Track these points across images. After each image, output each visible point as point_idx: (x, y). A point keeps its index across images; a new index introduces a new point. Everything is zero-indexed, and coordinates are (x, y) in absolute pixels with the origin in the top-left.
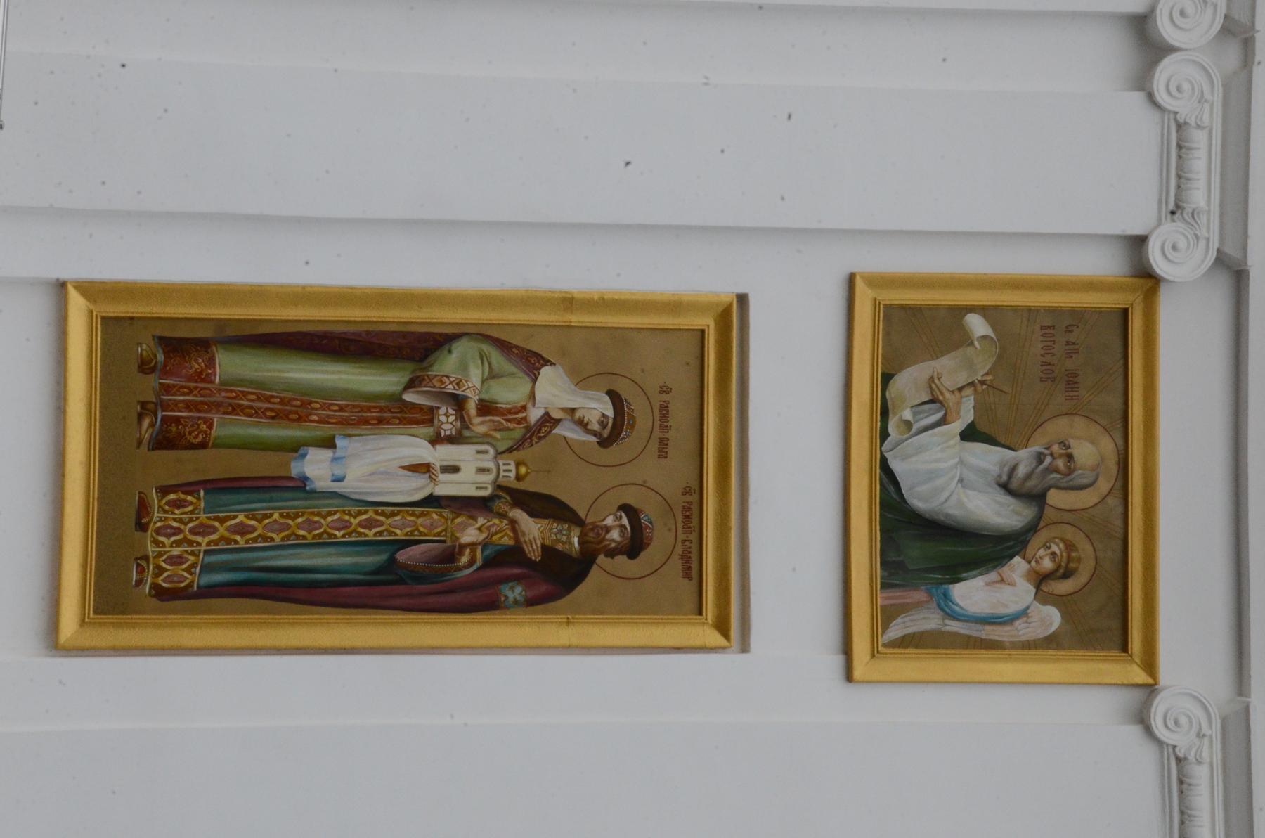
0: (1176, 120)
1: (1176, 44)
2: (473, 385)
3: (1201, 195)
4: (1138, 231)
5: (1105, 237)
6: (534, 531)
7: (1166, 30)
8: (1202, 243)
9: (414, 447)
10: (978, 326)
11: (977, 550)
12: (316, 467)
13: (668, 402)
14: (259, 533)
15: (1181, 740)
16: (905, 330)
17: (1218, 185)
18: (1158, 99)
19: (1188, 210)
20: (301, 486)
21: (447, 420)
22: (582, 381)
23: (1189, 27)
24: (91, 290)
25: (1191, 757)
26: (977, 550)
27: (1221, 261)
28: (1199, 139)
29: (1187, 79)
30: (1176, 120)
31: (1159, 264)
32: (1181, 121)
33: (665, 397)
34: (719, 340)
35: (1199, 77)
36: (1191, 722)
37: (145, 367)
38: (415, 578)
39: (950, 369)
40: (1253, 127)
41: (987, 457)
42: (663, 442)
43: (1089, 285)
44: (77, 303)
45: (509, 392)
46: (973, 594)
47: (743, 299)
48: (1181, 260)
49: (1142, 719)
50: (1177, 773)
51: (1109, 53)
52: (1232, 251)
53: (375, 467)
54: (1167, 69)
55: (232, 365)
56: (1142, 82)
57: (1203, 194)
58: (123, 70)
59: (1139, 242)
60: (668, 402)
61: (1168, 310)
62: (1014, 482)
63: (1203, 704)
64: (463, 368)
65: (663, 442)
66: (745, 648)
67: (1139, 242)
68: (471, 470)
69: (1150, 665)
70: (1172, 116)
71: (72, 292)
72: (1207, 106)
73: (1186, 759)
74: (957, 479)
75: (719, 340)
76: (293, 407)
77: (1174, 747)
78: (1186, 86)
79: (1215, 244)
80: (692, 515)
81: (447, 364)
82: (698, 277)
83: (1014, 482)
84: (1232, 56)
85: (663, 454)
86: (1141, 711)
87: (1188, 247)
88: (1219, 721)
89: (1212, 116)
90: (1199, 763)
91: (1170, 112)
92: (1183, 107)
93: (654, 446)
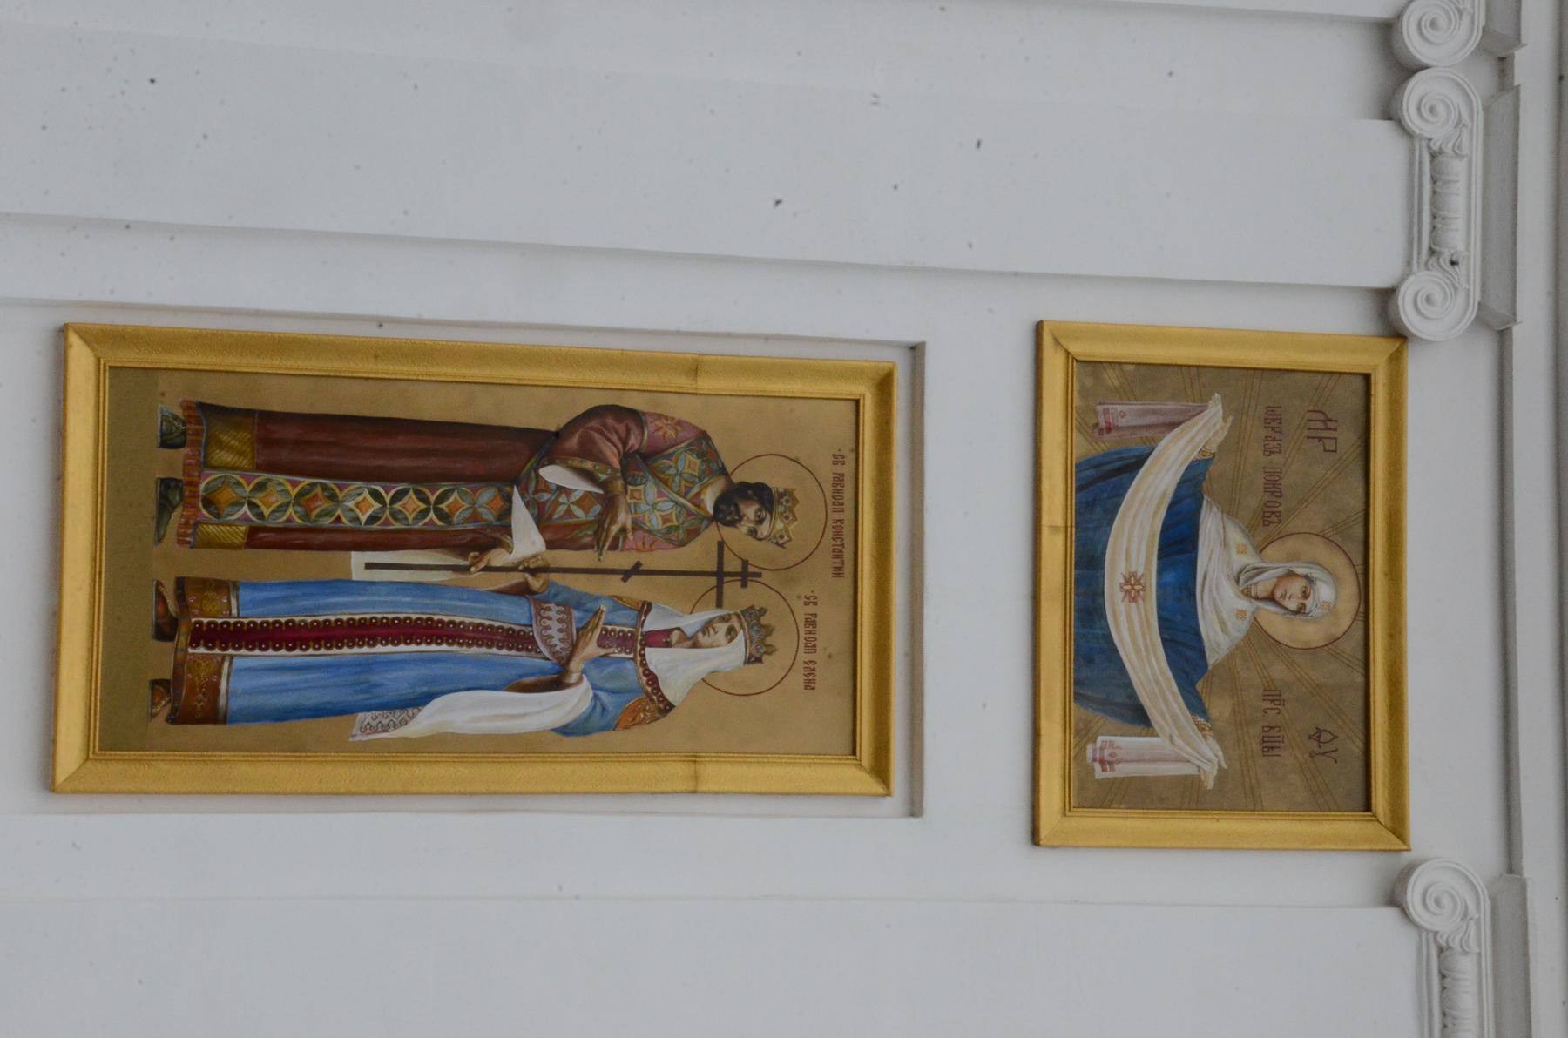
0: (1429, 147)
1: (1424, 60)
3: (1461, 236)
4: (1382, 282)
5: (1332, 20)
7: (1415, 44)
8: (1461, 296)
13: (815, 615)
15: (1441, 922)
17: (1479, 222)
18: (1418, 919)
19: (1446, 256)
23: (1444, 47)
24: (98, 338)
25: (1448, 149)
27: (1482, 320)
28: (1457, 169)
30: (1429, 147)
31: (1409, 317)
32: (1443, 943)
33: (811, 609)
34: (889, 393)
35: (1457, 98)
36: (1455, 903)
40: (1519, 268)
42: (810, 671)
44: (81, 360)
47: (916, 351)
48: (1437, 312)
49: (1393, 898)
50: (1440, 964)
51: (1348, 68)
52: (1498, 306)
54: (1416, 88)
57: (1461, 236)
58: (153, 76)
59: (1385, 297)
60: (815, 615)
61: (1419, 371)
62: (1227, 582)
63: (1463, 89)
65: (810, 671)
66: (914, 808)
67: (1385, 297)
69: (1398, 826)
70: (1424, 143)
71: (74, 339)
72: (1472, 925)
73: (1449, 948)
75: (889, 393)
77: (1436, 933)
78: (1446, 900)
79: (1481, 21)
80: (842, 494)
82: (867, 320)
83: (1227, 582)
85: (809, 685)
86: (1393, 891)
87: (1445, 298)
88: (1488, 903)
89: (1474, 146)
90: (1465, 953)
91: (1428, 931)
93: (797, 679)
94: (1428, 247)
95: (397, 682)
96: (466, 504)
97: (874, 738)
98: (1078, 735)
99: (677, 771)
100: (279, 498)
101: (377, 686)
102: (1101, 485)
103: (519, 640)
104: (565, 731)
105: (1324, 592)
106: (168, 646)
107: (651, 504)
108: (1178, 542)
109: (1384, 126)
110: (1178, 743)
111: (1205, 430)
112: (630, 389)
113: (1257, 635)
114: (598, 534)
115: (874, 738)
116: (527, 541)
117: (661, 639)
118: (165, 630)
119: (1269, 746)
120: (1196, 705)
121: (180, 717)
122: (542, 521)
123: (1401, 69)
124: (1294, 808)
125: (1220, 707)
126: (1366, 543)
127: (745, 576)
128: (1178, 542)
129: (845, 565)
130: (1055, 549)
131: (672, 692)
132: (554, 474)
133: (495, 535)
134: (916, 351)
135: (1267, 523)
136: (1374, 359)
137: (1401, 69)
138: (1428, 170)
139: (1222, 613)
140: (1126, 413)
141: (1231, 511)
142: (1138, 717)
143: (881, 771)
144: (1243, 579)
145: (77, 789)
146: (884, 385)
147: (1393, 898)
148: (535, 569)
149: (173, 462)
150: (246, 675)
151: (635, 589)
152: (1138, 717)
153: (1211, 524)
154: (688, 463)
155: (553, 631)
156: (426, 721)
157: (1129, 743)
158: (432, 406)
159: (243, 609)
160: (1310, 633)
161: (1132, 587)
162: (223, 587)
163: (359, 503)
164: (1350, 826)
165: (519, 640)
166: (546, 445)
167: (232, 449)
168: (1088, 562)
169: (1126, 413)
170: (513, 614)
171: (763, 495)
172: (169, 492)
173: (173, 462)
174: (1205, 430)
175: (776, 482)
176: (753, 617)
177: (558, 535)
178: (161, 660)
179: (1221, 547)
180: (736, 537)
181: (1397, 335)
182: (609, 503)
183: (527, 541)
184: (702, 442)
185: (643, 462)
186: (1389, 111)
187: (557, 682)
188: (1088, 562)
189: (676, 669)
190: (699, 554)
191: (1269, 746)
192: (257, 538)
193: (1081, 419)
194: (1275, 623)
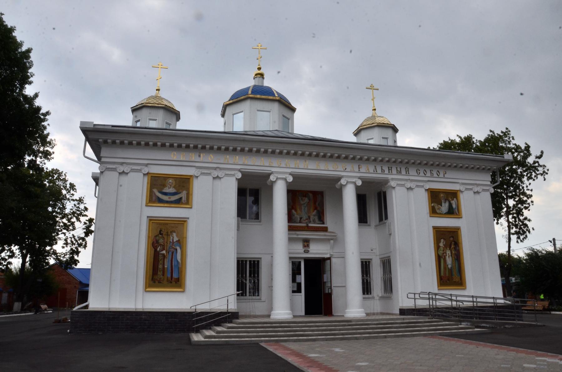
2: (442, 252)
3: (139, 168)
6: (453, 246)
9: (447, 257)
10: (433, 205)
11: (450, 205)
12: (450, 266)
14: (455, 272)
16: (434, 212)
20: (451, 268)
21: (445, 254)
22: (440, 242)
24: (146, 288)
26: (450, 205)
29: (126, 169)
31: (146, 172)
34: (151, 220)
37: (155, 282)
38: (458, 258)
39: (436, 207)
41: (443, 204)
43: (148, 180)
44: (148, 289)
45: (442, 249)
46: (454, 206)
47: (148, 217)
48: (146, 170)
49: (197, 177)
50: (203, 174)
53: (449, 261)
54: (220, 176)
55: (442, 274)
56: (220, 178)
57: (139, 168)
59: (144, 174)
61: (151, 171)
64: (441, 252)
66: (188, 218)
67: (144, 174)
68: (448, 252)
69: (191, 176)
74: (445, 207)
75: (151, 220)
76: (445, 268)
80: (160, 224)
81: (440, 254)
82: (145, 222)
84: (124, 165)
92: (223, 175)
94: (140, 171)
95: (176, 263)
96: (161, 257)
97: (182, 223)
98: (183, 204)
99: (184, 239)
100: (160, 273)
102: (160, 201)
103: (173, 253)
104: (181, 249)
105: (170, 181)
106: (398, 312)
107: (161, 241)
108: (166, 194)
109: (129, 174)
110: (183, 195)
111: (155, 191)
112: (151, 242)
113: (174, 187)
114: (164, 246)
115: (182, 223)
116: (164, 252)
117: (173, 240)
118: (171, 282)
119: (184, 187)
120: (180, 193)
121: (178, 281)
122: (162, 251)
123: (123, 172)
124: (189, 185)
125: (180, 191)
126: (166, 177)
127: (167, 233)
128: (166, 194)
129: (167, 224)
130: (166, 205)
131: (177, 239)
132: (158, 250)
133: (163, 254)
134: (148, 217)
135: (164, 186)
136: (150, 175)
137: (123, 172)
138: (133, 170)
139: (172, 190)
140: (154, 198)
141: (163, 189)
142: (181, 198)
143: (185, 221)
144: (169, 188)
145: (192, 205)
146: (150, 220)
147: (197, 177)
148: (166, 251)
149: (157, 282)
150: (175, 276)
151: (168, 243)
152: (181, 198)
153: (164, 191)
154: (157, 238)
155: (172, 250)
156: (179, 261)
157: (183, 199)
158: (152, 260)
159: (169, 276)
160: (174, 182)
161: (170, 198)
162: (168, 278)
163: (160, 266)
164: (191, 180)
165: (173, 253)
166: (156, 250)
167: (155, 277)
168: (167, 202)
169: (154, 198)
170: (170, 253)
171: (160, 231)
172: (159, 282)
173: (157, 282)
174: (155, 191)
175: (159, 230)
176: (171, 232)
177: (164, 249)
178: (174, 283)
179: (166, 190)
180: (164, 233)
181: (148, 173)
182: (161, 245)
183: (164, 252)
184: (156, 236)
185: (157, 242)
186: (127, 173)
187: (176, 250)
188: (167, 202)
189: (176, 239)
190: (165, 237)
191: (184, 187)
192: (163, 275)
193: (154, 202)
194: (173, 185)
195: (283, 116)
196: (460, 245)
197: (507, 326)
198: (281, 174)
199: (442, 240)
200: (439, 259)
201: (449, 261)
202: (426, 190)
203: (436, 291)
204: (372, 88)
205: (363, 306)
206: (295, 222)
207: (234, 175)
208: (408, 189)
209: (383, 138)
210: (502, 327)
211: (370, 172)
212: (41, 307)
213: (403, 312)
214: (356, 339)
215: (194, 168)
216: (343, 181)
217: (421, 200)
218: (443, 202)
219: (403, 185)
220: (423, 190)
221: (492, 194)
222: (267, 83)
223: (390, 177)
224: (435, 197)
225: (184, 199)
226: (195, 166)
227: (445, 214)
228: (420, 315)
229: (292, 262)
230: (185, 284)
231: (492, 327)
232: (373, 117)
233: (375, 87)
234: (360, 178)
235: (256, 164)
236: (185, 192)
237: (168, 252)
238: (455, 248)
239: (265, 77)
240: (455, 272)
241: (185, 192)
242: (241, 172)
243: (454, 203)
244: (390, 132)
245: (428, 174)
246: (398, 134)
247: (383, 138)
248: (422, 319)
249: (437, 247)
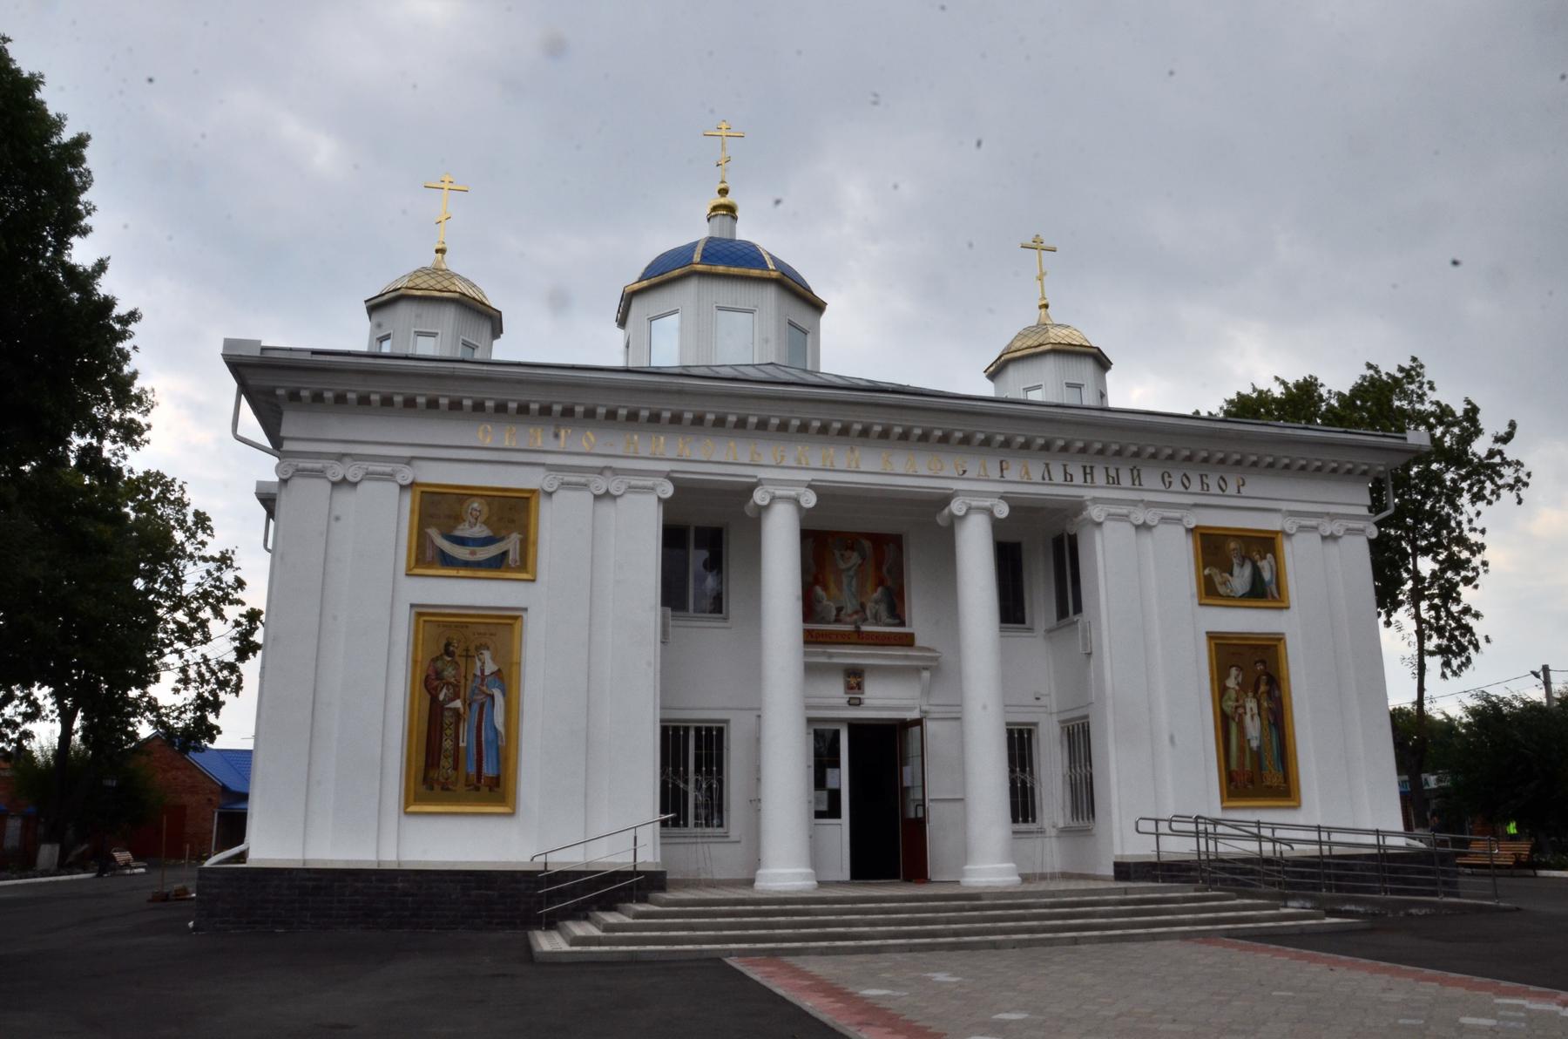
2: (1232, 704)
3: (387, 468)
6: (1263, 688)
9: (1248, 718)
10: (1207, 572)
11: (1257, 573)
12: (1254, 744)
14: (1270, 760)
16: (1210, 592)
20: (1259, 747)
21: (1241, 711)
22: (1228, 676)
24: (407, 804)
26: (1257, 573)
29: (352, 471)
31: (408, 482)
34: (422, 614)
37: (432, 788)
38: (1278, 719)
39: (1217, 579)
41: (1236, 570)
43: (413, 502)
44: (412, 809)
45: (1233, 695)
46: (1267, 575)
47: (412, 606)
48: (407, 475)
49: (550, 494)
50: (565, 485)
53: (1253, 728)
54: (612, 491)
55: (1234, 766)
56: (615, 498)
57: (387, 468)
59: (402, 487)
61: (423, 479)
64: (1229, 705)
66: (525, 610)
67: (402, 487)
68: (1251, 704)
69: (533, 491)
74: (1240, 579)
75: (422, 614)
76: (1241, 749)
80: (447, 625)
81: (1228, 710)
82: (404, 619)
84: (347, 460)
92: (623, 488)
94: (390, 477)
95: (491, 735)
96: (448, 719)
97: (507, 622)
98: (509, 569)
99: (514, 668)
100: (446, 763)
101: (859, 1013)
102: (447, 561)
103: (482, 707)
104: (504, 695)
105: (475, 505)
107: (449, 673)
108: (462, 541)
109: (359, 487)
110: (512, 544)
111: (433, 532)
112: (420, 676)
113: (485, 523)
114: (456, 686)
115: (507, 622)
116: (458, 704)
117: (482, 671)
118: (477, 789)
119: (513, 521)
120: (501, 539)
121: (498, 785)
122: (453, 700)
123: (344, 481)
124: (528, 516)
125: (503, 533)
126: (462, 495)
127: (467, 650)
128: (462, 541)
129: (466, 625)
130: (462, 573)
131: (495, 668)
132: (441, 697)
133: (456, 710)
134: (412, 606)
135: (458, 519)
136: (418, 490)
137: (344, 481)
138: (370, 476)
139: (480, 531)
140: (429, 553)
141: (454, 528)
142: (505, 554)
143: (516, 618)
144: (472, 526)
145: (535, 573)
146: (420, 614)
147: (550, 494)
148: (464, 702)
149: (437, 788)
150: (489, 770)
151: (470, 677)
152: (505, 554)
153: (458, 533)
154: (439, 664)
155: (480, 697)
156: (501, 728)
157: (511, 556)
158: (424, 727)
159: (472, 770)
160: (486, 510)
161: (473, 553)
162: (468, 775)
163: (448, 744)
164: (533, 503)
165: (482, 707)
166: (434, 699)
167: (434, 774)
168: (466, 564)
169: (429, 553)
170: (475, 707)
171: (448, 645)
172: (445, 788)
173: (437, 788)
174: (433, 532)
175: (444, 642)
176: (478, 648)
177: (456, 696)
178: (485, 789)
179: (464, 531)
180: (458, 652)
181: (413, 484)
182: (448, 684)
183: (458, 704)
184: (435, 660)
185: (439, 675)
186: (355, 484)
187: (492, 697)
188: (466, 564)
189: (490, 668)
190: (462, 661)
191: (513, 521)
192: (456, 768)
193: (430, 565)
194: (483, 518)
195: (791, 323)
196: (1284, 685)
197: (1413, 911)
198: (785, 487)
199: (1234, 671)
200: (1226, 723)
201: (1253, 728)
202: (1190, 531)
203: (1217, 813)
204: (1037, 245)
205: (1013, 855)
206: (823, 621)
207: (652, 489)
208: (1137, 527)
209: (1069, 385)
210: (1402, 913)
211: (1033, 480)
212: (114, 859)
213: (1124, 870)
214: (994, 945)
215: (541, 470)
216: (957, 507)
217: (1176, 557)
218: (1235, 563)
219: (1124, 518)
220: (1180, 531)
221: (1372, 543)
222: (745, 231)
223: (1088, 494)
224: (1215, 550)
225: (513, 556)
226: (543, 465)
227: (1243, 597)
228: (1173, 879)
229: (816, 732)
230: (515, 793)
231: (1374, 914)
232: (1042, 327)
233: (1046, 244)
234: (1004, 497)
235: (716, 459)
236: (515, 537)
237: (468, 704)
238: (1269, 693)
239: (738, 214)
240: (1270, 760)
241: (515, 537)
242: (672, 480)
243: (1266, 566)
244: (1087, 369)
245: (1195, 486)
246: (1109, 376)
247: (1069, 385)
248: (1176, 891)
249: (1220, 691)
